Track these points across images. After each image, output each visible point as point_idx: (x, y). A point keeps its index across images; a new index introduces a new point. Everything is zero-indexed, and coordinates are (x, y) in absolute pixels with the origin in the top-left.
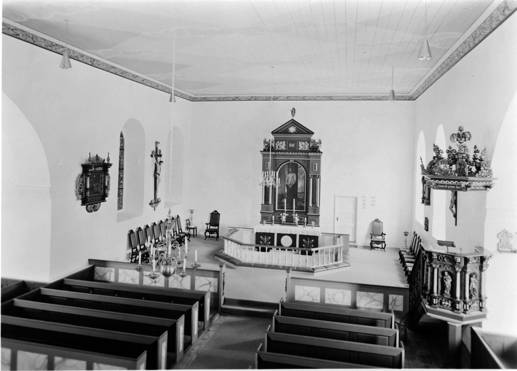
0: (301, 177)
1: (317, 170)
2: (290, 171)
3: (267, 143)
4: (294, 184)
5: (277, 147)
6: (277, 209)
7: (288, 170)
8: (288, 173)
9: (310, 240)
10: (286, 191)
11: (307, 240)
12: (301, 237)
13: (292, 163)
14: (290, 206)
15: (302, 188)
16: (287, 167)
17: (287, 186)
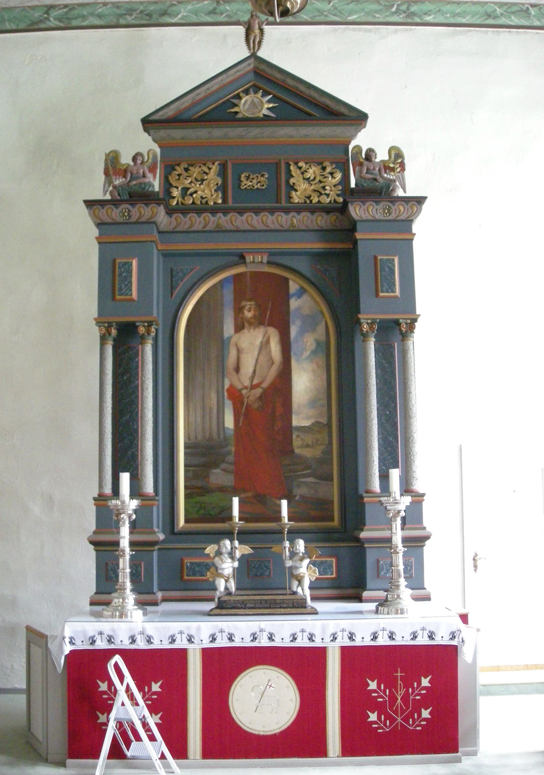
0: (305, 342)
1: (398, 293)
2: (248, 315)
3: (124, 172)
4: (273, 387)
5: (176, 193)
6: (181, 522)
7: (238, 310)
8: (239, 328)
9: (408, 684)
10: (229, 422)
11: (391, 684)
12: (356, 659)
13: (257, 276)
14: (260, 510)
15: (313, 403)
16: (228, 294)
17: (235, 395)
